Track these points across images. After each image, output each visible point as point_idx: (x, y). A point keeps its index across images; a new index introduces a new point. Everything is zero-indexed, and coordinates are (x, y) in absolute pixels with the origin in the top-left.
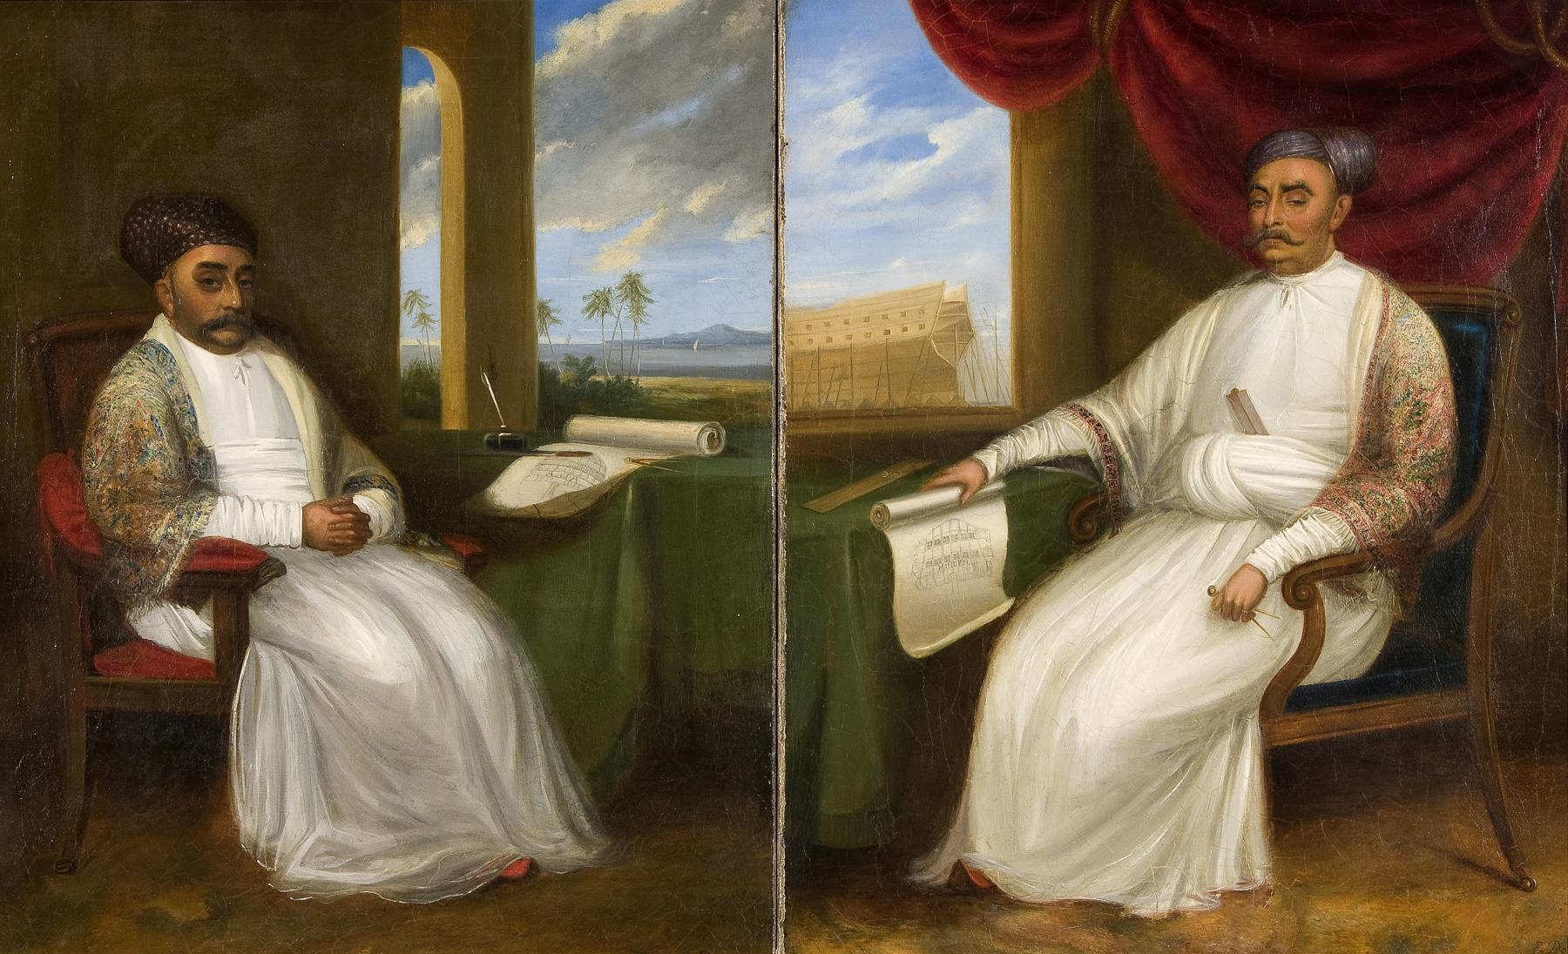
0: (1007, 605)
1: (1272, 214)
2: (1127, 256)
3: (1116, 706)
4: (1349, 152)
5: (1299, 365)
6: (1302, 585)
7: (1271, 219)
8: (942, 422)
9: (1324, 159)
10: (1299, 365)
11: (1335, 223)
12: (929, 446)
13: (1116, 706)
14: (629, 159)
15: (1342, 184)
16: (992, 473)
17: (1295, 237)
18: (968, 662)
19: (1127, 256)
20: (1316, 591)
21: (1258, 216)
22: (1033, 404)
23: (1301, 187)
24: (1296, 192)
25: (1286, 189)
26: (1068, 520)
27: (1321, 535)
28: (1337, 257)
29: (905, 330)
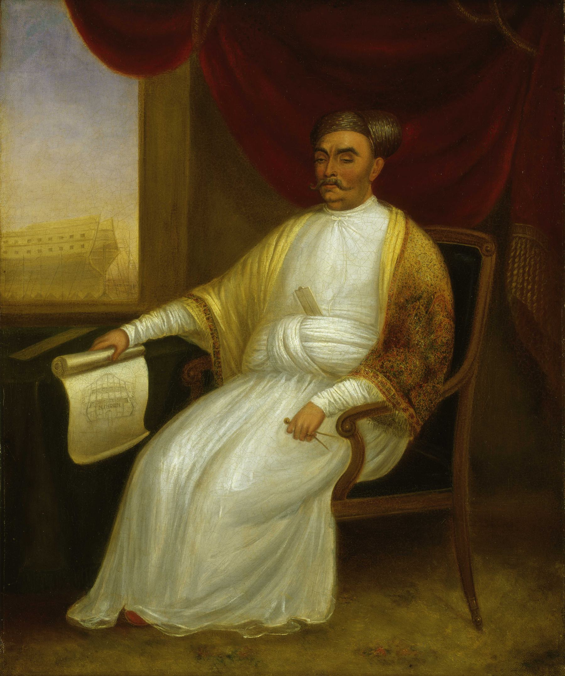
0: (147, 433)
1: (332, 168)
2: (228, 187)
3: (234, 490)
4: (384, 129)
5: (345, 262)
6: (349, 422)
7: (329, 172)
8: (102, 309)
9: (366, 132)
10: (345, 262)
11: (373, 176)
12: (93, 326)
13: (234, 490)
14: (283, 381)
15: (380, 149)
16: (132, 343)
17: (344, 184)
18: (116, 473)
19: (228, 187)
20: (296, 375)
21: (320, 168)
22: (156, 290)
23: (350, 151)
24: (348, 153)
25: (341, 152)
26: (184, 377)
27: (354, 391)
28: (371, 201)
29: (83, 246)
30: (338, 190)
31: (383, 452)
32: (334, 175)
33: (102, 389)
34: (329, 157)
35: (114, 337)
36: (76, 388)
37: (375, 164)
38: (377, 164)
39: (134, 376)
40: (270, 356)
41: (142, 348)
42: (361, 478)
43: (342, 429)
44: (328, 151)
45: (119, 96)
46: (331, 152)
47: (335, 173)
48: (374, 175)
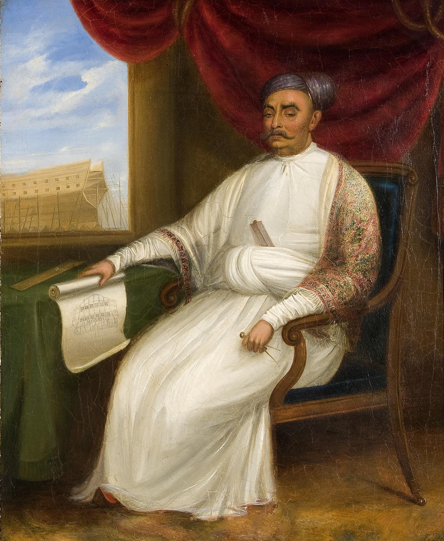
1: (276, 121)
3: (188, 401)
4: (320, 86)
6: (293, 332)
7: (276, 124)
9: (306, 90)
11: (312, 126)
13: (188, 401)
15: (316, 104)
16: (117, 268)
17: (289, 134)
18: (103, 376)
21: (268, 122)
23: (293, 106)
24: (290, 109)
25: (284, 107)
26: (161, 295)
28: (313, 146)
30: (283, 139)
31: (322, 360)
32: (279, 127)
33: (90, 311)
34: (276, 112)
35: (103, 267)
36: (71, 311)
37: (313, 117)
38: (315, 117)
39: (117, 299)
40: (226, 281)
41: (122, 275)
42: (302, 383)
43: (289, 337)
44: (274, 106)
45: (109, 76)
46: (276, 106)
47: (280, 125)
48: (312, 125)
